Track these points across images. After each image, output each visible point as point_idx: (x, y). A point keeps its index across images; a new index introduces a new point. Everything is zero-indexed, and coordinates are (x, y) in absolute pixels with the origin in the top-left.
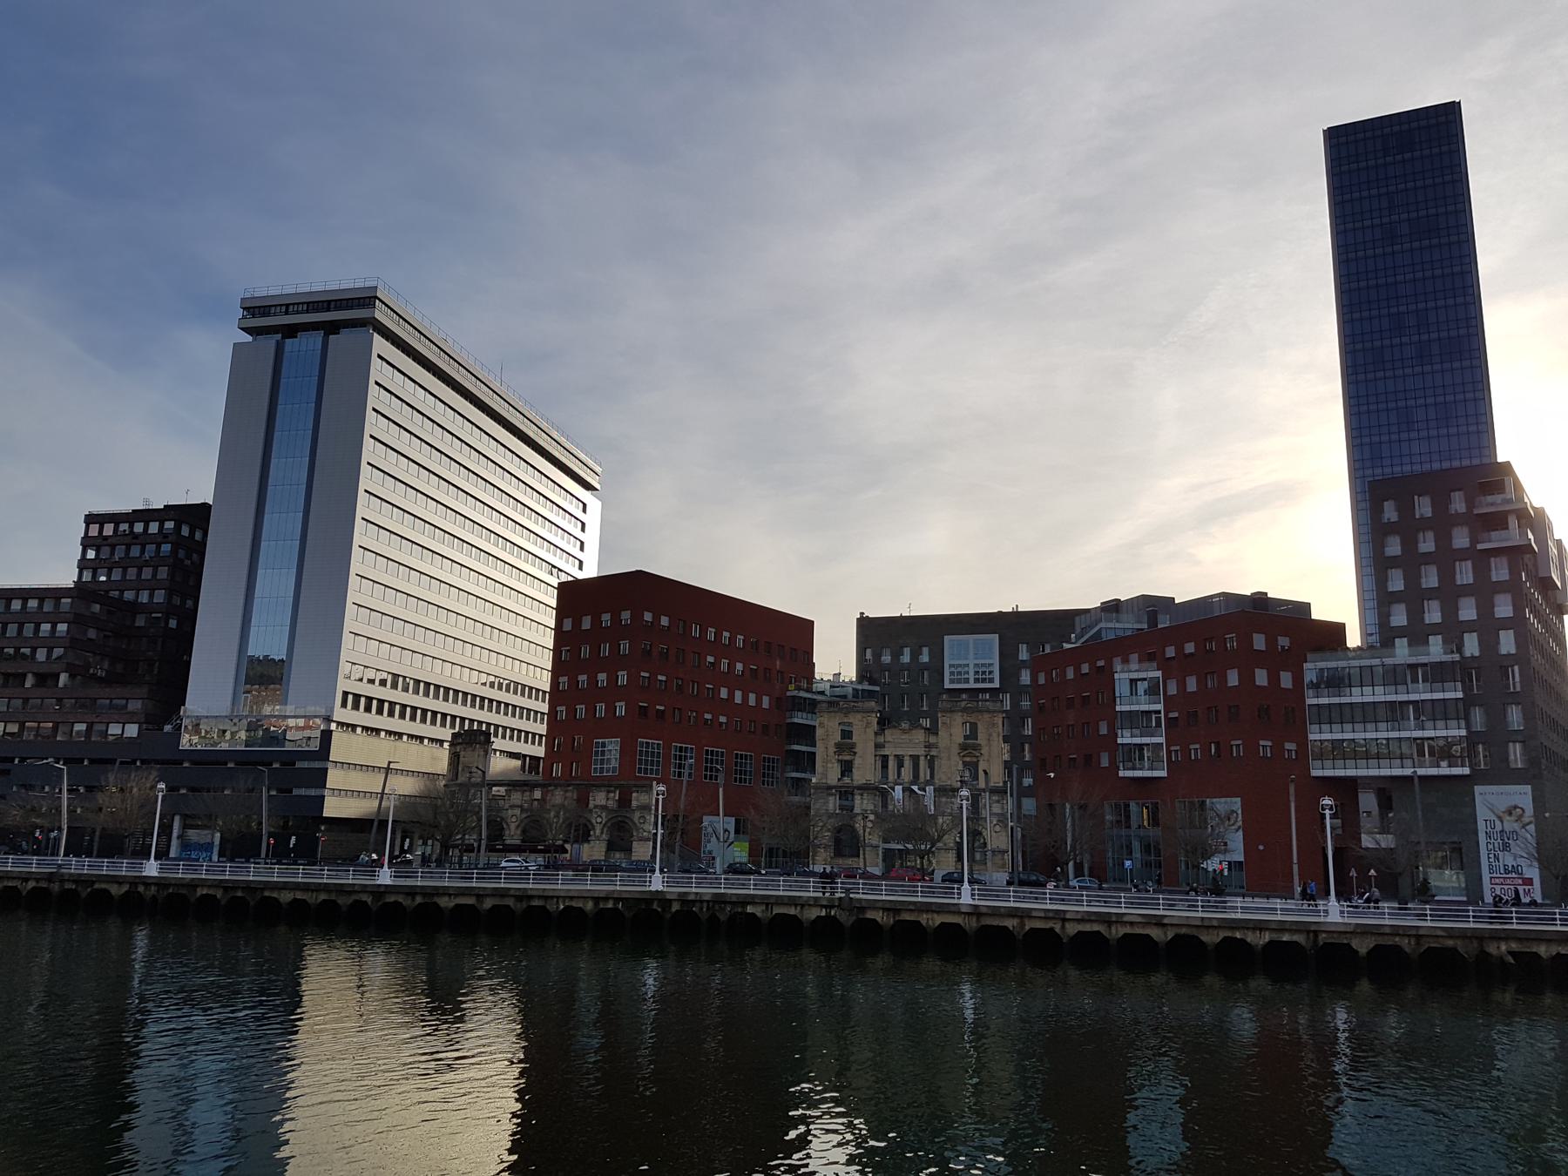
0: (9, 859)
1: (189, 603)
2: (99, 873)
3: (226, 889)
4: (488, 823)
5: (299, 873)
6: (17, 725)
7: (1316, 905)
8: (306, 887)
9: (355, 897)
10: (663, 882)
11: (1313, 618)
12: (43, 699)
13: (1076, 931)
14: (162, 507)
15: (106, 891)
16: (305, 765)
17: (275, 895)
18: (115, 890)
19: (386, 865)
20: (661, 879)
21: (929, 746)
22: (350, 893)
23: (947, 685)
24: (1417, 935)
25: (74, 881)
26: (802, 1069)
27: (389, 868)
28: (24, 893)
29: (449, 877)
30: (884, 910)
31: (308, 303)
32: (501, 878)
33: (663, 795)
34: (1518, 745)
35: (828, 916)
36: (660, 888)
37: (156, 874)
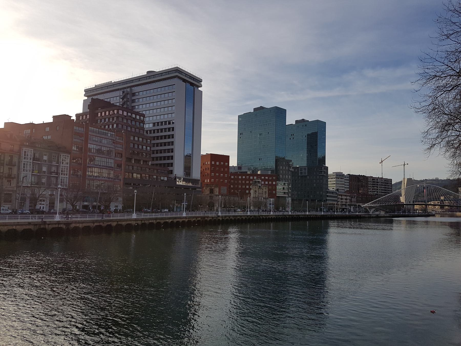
1: (226, 164)
3: (241, 217)
7: (68, 216)
11: (52, 121)
14: (51, 120)
16: (198, 190)
19: (134, 213)
23: (299, 175)
24: (255, 216)
26: (243, 252)
29: (97, 217)
33: (60, 189)
34: (113, 160)
37: (185, 216)
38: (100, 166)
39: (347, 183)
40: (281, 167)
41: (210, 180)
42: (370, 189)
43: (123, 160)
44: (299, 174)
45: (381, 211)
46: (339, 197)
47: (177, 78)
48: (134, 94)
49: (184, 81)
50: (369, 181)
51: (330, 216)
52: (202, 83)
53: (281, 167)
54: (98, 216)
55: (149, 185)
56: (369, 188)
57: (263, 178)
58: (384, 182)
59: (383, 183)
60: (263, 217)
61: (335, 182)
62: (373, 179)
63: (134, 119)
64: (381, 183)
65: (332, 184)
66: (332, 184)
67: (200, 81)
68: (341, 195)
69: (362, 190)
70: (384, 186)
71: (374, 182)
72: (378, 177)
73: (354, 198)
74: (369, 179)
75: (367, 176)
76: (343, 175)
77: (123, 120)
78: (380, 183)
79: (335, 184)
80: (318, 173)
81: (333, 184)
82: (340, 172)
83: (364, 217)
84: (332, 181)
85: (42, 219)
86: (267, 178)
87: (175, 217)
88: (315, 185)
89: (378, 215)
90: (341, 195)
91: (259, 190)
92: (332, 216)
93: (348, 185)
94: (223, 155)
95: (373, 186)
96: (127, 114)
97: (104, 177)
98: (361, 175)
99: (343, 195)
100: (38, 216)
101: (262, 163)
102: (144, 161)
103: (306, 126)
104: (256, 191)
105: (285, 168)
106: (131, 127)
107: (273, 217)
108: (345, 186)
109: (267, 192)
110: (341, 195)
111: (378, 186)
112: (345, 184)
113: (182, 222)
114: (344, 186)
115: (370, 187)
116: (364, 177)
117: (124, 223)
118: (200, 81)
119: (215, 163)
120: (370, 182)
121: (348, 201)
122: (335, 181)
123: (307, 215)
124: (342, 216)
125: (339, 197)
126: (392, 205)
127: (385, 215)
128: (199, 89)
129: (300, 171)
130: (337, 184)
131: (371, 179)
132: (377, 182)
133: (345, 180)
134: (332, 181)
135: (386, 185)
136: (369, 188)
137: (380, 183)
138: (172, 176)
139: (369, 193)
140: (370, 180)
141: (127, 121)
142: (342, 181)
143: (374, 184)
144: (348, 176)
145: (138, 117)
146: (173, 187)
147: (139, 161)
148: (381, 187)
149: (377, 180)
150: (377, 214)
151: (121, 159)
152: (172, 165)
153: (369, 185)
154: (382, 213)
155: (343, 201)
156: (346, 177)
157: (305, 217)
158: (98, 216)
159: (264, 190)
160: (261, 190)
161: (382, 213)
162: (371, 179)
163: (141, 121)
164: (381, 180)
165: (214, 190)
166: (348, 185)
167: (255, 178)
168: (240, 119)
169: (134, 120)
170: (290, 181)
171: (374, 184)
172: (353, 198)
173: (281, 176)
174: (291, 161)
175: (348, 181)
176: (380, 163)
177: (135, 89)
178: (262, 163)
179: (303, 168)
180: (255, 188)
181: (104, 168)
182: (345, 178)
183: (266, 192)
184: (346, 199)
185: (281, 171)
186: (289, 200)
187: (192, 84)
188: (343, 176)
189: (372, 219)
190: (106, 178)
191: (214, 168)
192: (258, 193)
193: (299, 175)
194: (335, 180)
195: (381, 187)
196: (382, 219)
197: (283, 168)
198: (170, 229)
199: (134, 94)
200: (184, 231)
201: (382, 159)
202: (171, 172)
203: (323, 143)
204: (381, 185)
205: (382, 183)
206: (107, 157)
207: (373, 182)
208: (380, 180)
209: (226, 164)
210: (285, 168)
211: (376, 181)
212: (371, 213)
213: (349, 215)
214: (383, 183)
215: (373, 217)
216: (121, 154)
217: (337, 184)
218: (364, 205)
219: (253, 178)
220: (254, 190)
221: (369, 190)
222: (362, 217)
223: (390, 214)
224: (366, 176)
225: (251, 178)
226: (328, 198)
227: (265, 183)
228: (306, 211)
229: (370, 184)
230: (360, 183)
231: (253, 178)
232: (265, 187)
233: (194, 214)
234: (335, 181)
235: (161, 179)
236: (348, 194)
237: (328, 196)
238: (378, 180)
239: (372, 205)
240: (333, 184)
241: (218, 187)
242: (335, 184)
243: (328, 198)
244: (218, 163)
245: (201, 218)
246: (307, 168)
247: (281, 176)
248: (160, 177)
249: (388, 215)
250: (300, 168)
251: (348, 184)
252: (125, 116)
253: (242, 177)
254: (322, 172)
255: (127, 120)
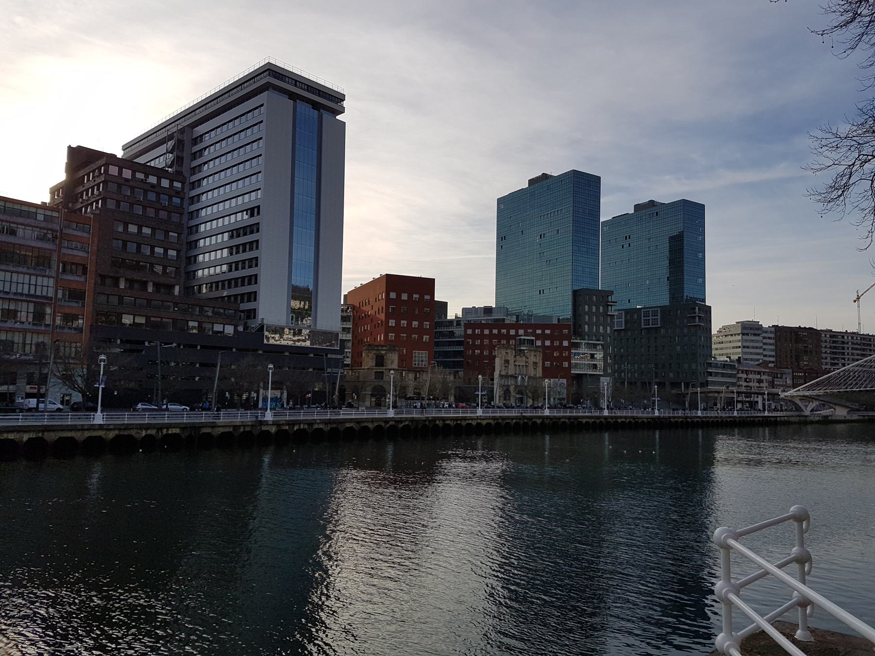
0: (165, 414)
2: (143, 422)
4: (339, 389)
5: (45, 419)
6: (145, 318)
8: (73, 428)
9: (468, 422)
10: (103, 418)
12: (163, 301)
13: (57, 437)
15: (367, 427)
16: (334, 356)
17: (581, 420)
18: (371, 426)
19: (269, 410)
20: (102, 417)
21: (526, 362)
22: (465, 420)
23: (643, 327)
25: (288, 424)
27: (101, 413)
28: (512, 424)
30: (492, 419)
31: (308, 86)
32: (45, 419)
33: (104, 362)
35: (457, 424)
36: (548, 414)
38: (7, 293)
39: (770, 344)
40: (586, 307)
41: (386, 336)
42: (826, 358)
43: (89, 283)
44: (643, 324)
45: (838, 408)
46: (740, 375)
47: (271, 89)
48: (196, 141)
49: (292, 96)
50: (823, 339)
51: (681, 420)
52: (345, 104)
53: (586, 307)
54: (151, 415)
55: (175, 345)
56: (824, 355)
57: (539, 332)
58: (859, 342)
59: (857, 344)
60: (609, 420)
61: (740, 344)
62: (833, 335)
63: (153, 186)
64: (853, 343)
65: (733, 348)
66: (733, 348)
67: (339, 98)
68: (746, 371)
69: (806, 361)
70: (859, 352)
71: (834, 342)
72: (844, 331)
73: (781, 378)
74: (823, 335)
75: (819, 329)
76: (760, 327)
77: (145, 195)
78: (850, 343)
79: (740, 347)
80: (685, 321)
81: (737, 347)
82: (752, 321)
83: (787, 423)
84: (733, 341)
85: (522, 413)
86: (548, 332)
87: (379, 418)
88: (679, 348)
89: (826, 417)
90: (747, 372)
91: (518, 358)
92: (689, 420)
93: (771, 350)
94: (421, 278)
95: (833, 351)
96: (133, 175)
97: (23, 323)
98: (805, 328)
99: (752, 371)
100: (250, 413)
101: (544, 301)
102: (157, 285)
103: (657, 215)
104: (507, 362)
105: (598, 309)
106: (143, 206)
107: (484, 422)
108: (765, 353)
109: (540, 364)
110: (747, 372)
111: (846, 351)
112: (765, 347)
113: (466, 425)
114: (761, 351)
115: (826, 353)
116: (812, 331)
117: (51, 437)
118: (339, 98)
119: (399, 296)
120: (826, 341)
121: (764, 385)
122: (739, 341)
123: (606, 418)
124: (720, 420)
125: (740, 375)
126: (855, 391)
127: (848, 418)
128: (338, 117)
129: (643, 318)
130: (744, 347)
131: (828, 336)
132: (843, 343)
133: (764, 338)
134: (733, 341)
135: (864, 350)
136: (824, 355)
137: (850, 343)
138: (254, 324)
139: (824, 367)
140: (826, 338)
141: (133, 192)
142: (757, 341)
143: (835, 347)
144: (773, 329)
145: (152, 180)
146: (257, 350)
147: (144, 284)
148: (853, 354)
149: (843, 337)
150: (824, 414)
151: (82, 279)
152: (253, 296)
153: (824, 350)
154: (841, 413)
155: (750, 384)
156: (766, 332)
157: (598, 421)
158: (151, 415)
159: (532, 359)
160: (524, 358)
161: (841, 413)
162: (828, 336)
163: (173, 193)
164: (852, 338)
165: (385, 357)
166: (771, 350)
167: (521, 332)
168: (502, 206)
169: (152, 189)
170: (610, 339)
171: (835, 347)
172: (777, 378)
173: (586, 327)
174: (612, 293)
175: (772, 341)
176: (855, 301)
177: (201, 129)
178: (544, 301)
179: (650, 310)
180: (507, 353)
181: (22, 301)
182: (764, 335)
183: (535, 363)
184: (760, 381)
185: (587, 317)
186: (605, 382)
187: (316, 106)
188: (758, 329)
189: (810, 428)
190: (26, 323)
191: (394, 309)
192: (513, 366)
193: (643, 327)
194: (740, 337)
195: (853, 354)
196: (840, 427)
197: (590, 309)
198: (24, 463)
199: (196, 141)
200: (498, 441)
201: (857, 292)
202: (252, 314)
203: (700, 252)
204: (852, 349)
205: (855, 344)
206: (32, 271)
207: (833, 343)
208: (850, 338)
209: (427, 297)
210: (598, 309)
211: (840, 339)
212: (807, 412)
213: (740, 417)
214: (857, 344)
215: (812, 422)
216: (84, 265)
217: (744, 347)
218: (786, 394)
219: (517, 332)
220: (501, 358)
221: (823, 361)
222: (781, 421)
223: (861, 413)
224: (817, 330)
225: (512, 332)
226: (710, 379)
227: (543, 343)
228: (694, 406)
229: (826, 347)
230: (800, 346)
231: (517, 332)
232: (533, 353)
233: (126, 418)
234: (739, 341)
235: (214, 329)
236: (764, 370)
237: (710, 374)
238: (846, 338)
239: (807, 393)
240: (737, 347)
241: (394, 350)
242: (740, 347)
243: (710, 379)
244: (404, 297)
245: (395, 421)
246: (659, 309)
247: (586, 327)
248: (210, 326)
249: (858, 417)
250: (643, 310)
251: (773, 347)
252: (127, 180)
253: (491, 332)
254: (694, 317)
255: (132, 188)
